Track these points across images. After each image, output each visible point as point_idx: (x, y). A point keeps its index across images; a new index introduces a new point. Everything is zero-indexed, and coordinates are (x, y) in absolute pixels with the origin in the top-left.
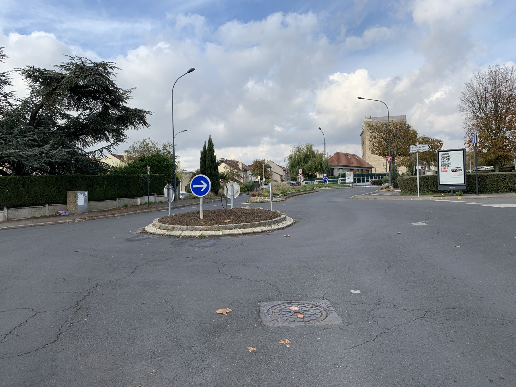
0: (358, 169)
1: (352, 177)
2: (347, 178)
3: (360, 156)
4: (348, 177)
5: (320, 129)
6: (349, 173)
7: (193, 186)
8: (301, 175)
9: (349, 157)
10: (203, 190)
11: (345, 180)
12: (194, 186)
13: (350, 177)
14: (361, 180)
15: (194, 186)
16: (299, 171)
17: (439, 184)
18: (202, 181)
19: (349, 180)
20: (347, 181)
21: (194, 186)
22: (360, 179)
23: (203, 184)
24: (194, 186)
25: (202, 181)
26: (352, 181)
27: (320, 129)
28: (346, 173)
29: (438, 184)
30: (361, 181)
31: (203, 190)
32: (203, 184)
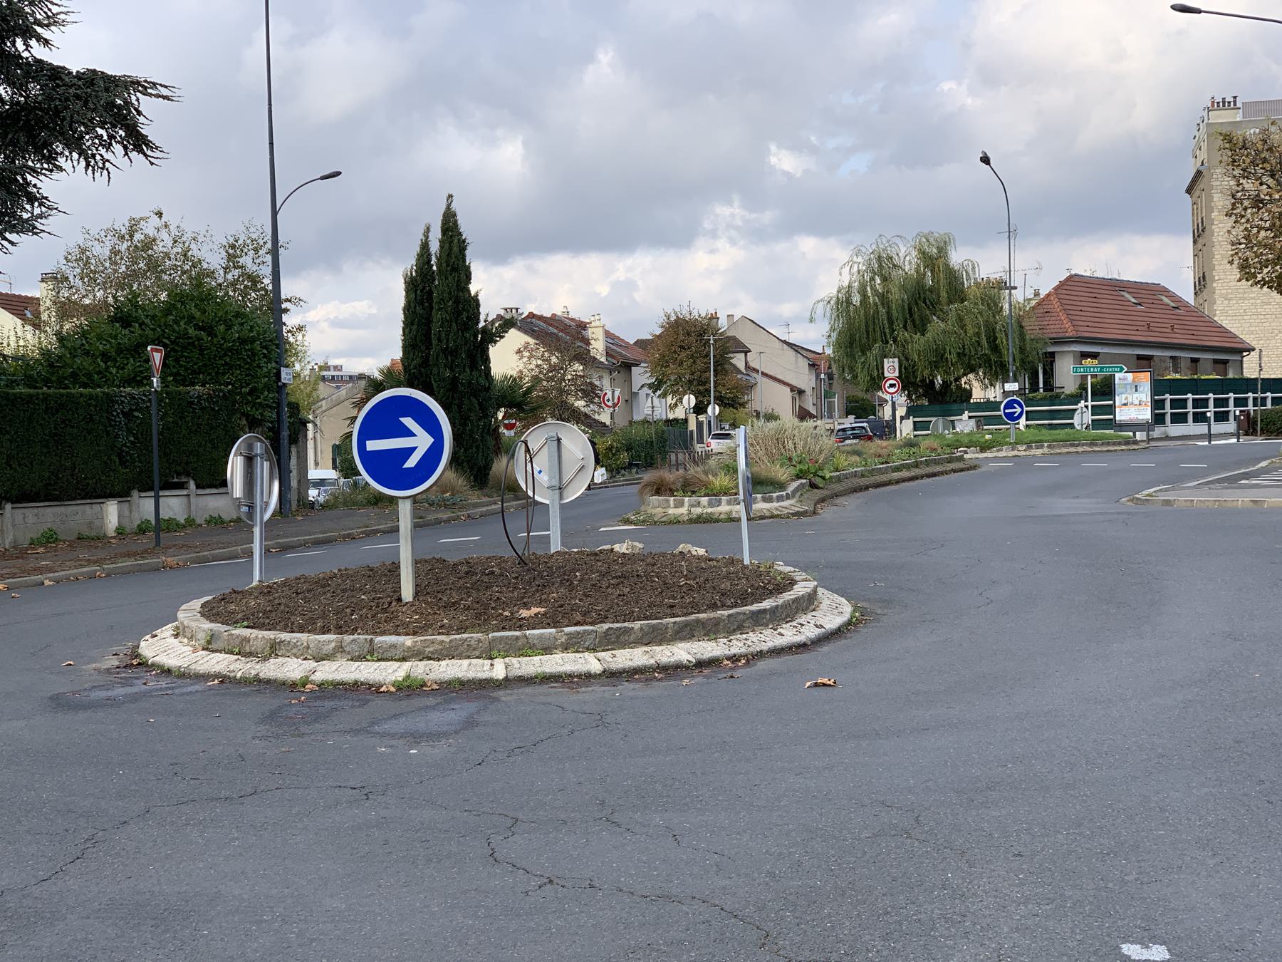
0: (1171, 357)
1: (1145, 394)
2: (1119, 400)
4: (1124, 396)
5: (985, 160)
6: (1130, 376)
8: (892, 386)
10: (411, 462)
11: (1111, 409)
12: (372, 445)
13: (1136, 397)
18: (1015, 405)
20: (1122, 415)
22: (1183, 403)
24: (372, 445)
26: (1146, 414)
28: (1117, 376)
30: (1168, 418)
31: (411, 462)
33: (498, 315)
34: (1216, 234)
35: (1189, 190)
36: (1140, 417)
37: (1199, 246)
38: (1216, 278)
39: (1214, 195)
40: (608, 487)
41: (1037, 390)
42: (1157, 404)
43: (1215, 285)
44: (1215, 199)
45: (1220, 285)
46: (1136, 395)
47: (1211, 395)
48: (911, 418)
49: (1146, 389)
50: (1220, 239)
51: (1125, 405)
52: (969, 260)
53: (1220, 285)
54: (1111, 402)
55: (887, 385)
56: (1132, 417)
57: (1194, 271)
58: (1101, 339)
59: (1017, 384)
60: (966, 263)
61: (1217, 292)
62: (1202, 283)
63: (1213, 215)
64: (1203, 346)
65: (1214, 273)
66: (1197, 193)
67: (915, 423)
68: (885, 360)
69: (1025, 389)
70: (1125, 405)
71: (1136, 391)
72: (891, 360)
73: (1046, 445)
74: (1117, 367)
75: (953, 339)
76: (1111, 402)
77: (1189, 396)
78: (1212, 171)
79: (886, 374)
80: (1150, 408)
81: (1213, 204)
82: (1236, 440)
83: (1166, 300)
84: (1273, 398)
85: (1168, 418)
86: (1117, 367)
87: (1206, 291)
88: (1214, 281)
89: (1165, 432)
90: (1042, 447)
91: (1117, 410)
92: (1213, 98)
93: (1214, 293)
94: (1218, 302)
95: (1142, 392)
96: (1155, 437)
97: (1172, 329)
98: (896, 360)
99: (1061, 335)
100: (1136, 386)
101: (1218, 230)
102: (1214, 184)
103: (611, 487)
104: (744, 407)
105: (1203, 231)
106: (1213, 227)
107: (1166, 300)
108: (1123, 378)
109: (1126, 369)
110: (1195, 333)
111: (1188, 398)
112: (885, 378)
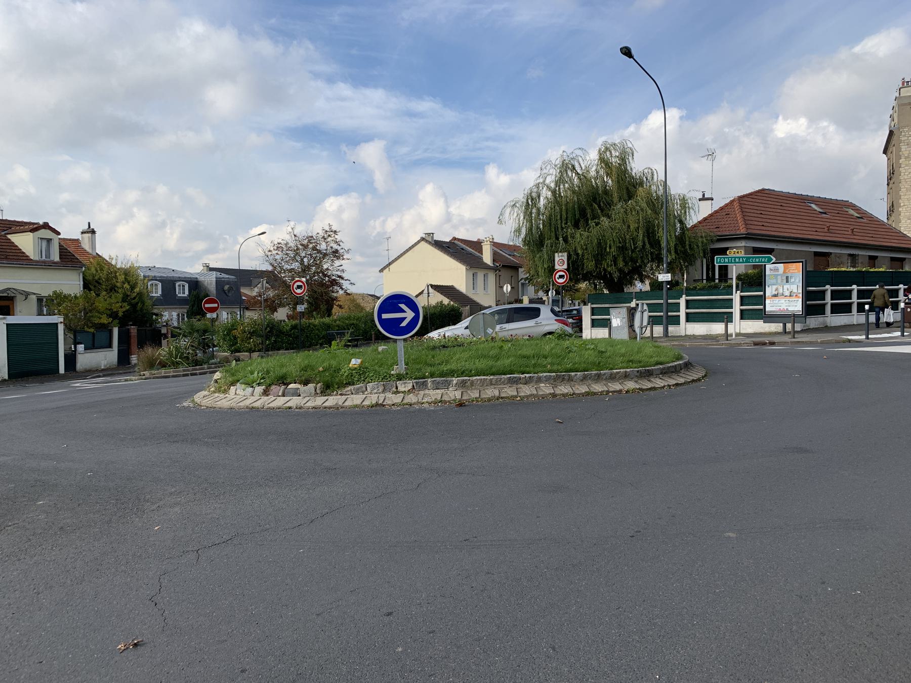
0: (850, 255)
1: (796, 286)
2: (769, 291)
3: (881, 214)
4: (774, 287)
5: (627, 52)
6: (781, 266)
7: (381, 317)
8: (561, 277)
9: (813, 206)
10: (404, 324)
11: (762, 300)
12: (385, 316)
13: (787, 289)
14: (828, 300)
15: (383, 315)
16: (557, 259)
17: (765, 314)
18: (403, 306)
19: (783, 301)
20: (771, 306)
21: (383, 315)
22: (848, 295)
23: (404, 311)
24: (385, 316)
25: (403, 306)
26: (796, 306)
27: (627, 52)
28: (768, 267)
29: (764, 314)
30: (828, 309)
31: (404, 324)
32: (404, 311)
33: (421, 238)
34: (902, 174)
35: (885, 152)
36: (791, 309)
37: (890, 185)
38: (902, 204)
39: (902, 147)
40: (195, 374)
41: (714, 280)
42: (808, 296)
43: (900, 209)
44: (902, 150)
45: (904, 209)
46: (786, 287)
47: (828, 287)
48: (589, 304)
49: (797, 281)
50: (906, 177)
51: (775, 296)
52: (649, 168)
53: (904, 209)
54: (762, 293)
55: (557, 276)
56: (782, 308)
57: (888, 204)
58: (763, 235)
59: (670, 275)
60: (646, 171)
61: (902, 214)
62: (891, 210)
63: (901, 161)
64: (880, 246)
65: (900, 201)
66: (889, 152)
67: (593, 309)
68: (556, 255)
69: (703, 280)
70: (775, 296)
71: (787, 282)
72: (560, 254)
73: (455, 380)
74: (765, 257)
75: (614, 234)
76: (762, 293)
77: (854, 287)
78: (901, 130)
79: (557, 267)
80: (800, 300)
81: (901, 153)
82: (899, 334)
83: (852, 212)
84: (832, 291)
85: (828, 309)
86: (765, 257)
87: (893, 215)
88: (900, 207)
89: (825, 322)
90: (447, 385)
91: (768, 301)
92: (903, 79)
93: (900, 215)
94: (903, 221)
95: (793, 283)
96: (811, 327)
97: (853, 232)
98: (565, 254)
99: (732, 233)
100: (787, 278)
101: (904, 171)
102: (903, 139)
103: (173, 376)
104: (579, 291)
105: (893, 174)
106: (901, 169)
107: (852, 212)
108: (773, 270)
109: (774, 260)
110: (874, 236)
111: (853, 289)
112: (556, 270)
